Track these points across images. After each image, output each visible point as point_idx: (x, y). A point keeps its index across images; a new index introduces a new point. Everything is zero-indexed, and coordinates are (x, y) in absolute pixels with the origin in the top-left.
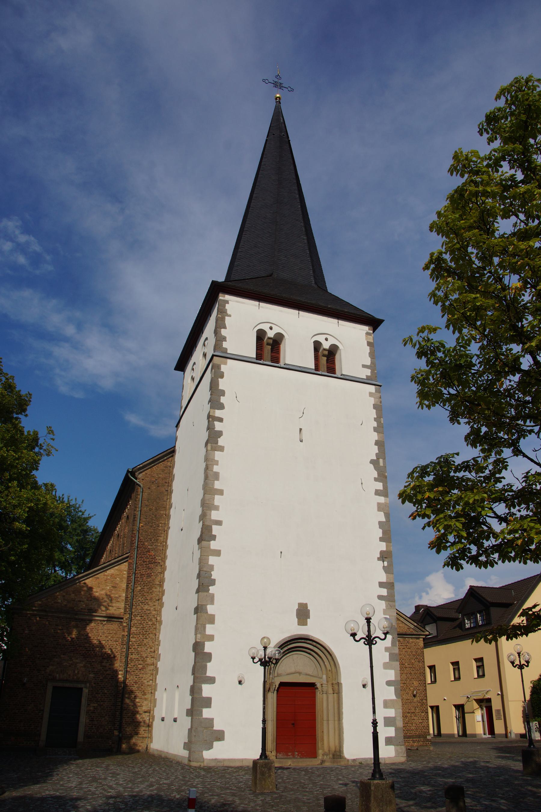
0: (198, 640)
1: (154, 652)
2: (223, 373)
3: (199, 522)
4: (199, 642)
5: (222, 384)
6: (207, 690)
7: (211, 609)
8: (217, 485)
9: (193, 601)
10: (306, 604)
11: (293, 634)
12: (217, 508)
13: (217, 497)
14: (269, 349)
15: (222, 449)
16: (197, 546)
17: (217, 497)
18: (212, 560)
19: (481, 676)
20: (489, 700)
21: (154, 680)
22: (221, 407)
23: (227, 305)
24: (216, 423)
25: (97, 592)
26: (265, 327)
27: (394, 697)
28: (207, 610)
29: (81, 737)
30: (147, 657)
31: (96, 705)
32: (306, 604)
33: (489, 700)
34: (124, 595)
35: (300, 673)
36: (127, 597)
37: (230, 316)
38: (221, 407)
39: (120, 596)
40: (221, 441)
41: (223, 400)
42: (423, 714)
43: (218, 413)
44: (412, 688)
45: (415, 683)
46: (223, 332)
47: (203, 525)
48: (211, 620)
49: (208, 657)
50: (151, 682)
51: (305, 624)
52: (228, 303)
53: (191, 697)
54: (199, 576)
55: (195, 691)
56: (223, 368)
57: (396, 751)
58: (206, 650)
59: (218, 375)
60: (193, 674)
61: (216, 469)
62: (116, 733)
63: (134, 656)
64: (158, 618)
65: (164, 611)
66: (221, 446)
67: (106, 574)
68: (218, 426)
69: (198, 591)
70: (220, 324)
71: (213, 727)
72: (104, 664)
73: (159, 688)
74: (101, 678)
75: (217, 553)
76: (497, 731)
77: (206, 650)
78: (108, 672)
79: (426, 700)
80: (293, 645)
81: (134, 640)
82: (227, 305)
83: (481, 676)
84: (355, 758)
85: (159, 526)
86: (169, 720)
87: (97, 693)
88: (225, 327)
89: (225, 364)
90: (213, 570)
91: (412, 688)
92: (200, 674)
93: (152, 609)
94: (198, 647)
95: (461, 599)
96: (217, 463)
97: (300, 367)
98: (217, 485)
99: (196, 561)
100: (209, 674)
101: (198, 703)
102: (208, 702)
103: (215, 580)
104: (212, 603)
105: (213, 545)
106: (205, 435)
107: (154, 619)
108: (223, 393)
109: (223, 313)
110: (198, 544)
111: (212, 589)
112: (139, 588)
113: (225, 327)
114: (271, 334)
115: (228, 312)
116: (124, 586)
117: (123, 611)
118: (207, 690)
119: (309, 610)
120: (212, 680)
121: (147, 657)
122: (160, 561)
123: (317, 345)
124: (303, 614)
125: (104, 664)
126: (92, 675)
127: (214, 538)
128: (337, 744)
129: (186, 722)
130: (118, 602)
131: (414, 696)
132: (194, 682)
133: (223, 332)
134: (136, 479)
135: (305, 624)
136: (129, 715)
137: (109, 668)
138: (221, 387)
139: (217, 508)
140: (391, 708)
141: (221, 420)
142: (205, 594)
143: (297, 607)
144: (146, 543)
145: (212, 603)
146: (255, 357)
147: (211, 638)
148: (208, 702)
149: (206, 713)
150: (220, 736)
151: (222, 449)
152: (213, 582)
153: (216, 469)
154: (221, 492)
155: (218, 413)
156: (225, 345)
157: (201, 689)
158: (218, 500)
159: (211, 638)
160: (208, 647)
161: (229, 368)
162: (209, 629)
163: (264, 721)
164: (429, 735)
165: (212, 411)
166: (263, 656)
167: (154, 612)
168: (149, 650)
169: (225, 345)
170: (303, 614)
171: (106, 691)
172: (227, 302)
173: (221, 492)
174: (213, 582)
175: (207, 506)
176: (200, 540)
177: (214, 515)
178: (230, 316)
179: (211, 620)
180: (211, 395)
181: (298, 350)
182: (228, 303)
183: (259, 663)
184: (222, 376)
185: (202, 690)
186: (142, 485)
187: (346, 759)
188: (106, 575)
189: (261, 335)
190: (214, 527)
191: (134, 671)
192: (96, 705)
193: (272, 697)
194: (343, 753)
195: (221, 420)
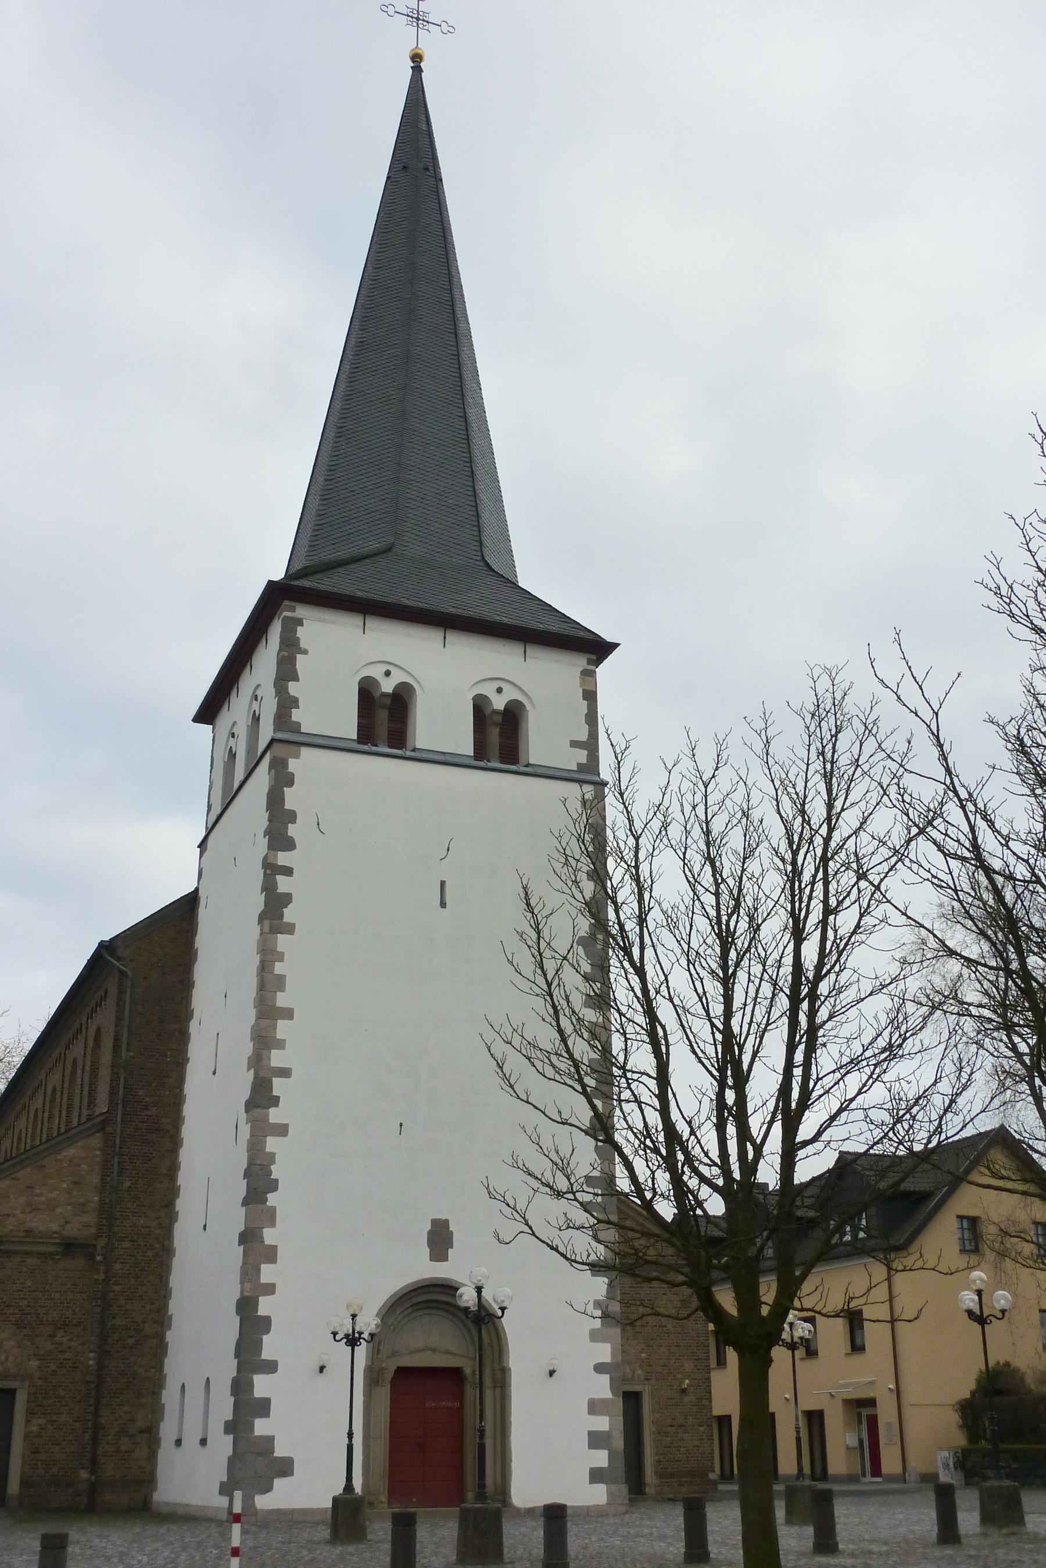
0: (246, 1294)
1: (159, 1311)
2: (293, 775)
3: (249, 1070)
4: (248, 1298)
5: (292, 798)
6: (262, 1385)
7: (270, 1236)
8: (282, 1000)
9: (237, 1219)
10: (446, 1222)
11: (421, 1278)
12: (281, 1045)
13: (280, 1023)
14: (385, 719)
15: (290, 929)
16: (243, 1116)
17: (280, 1023)
18: (272, 1144)
19: (857, 1347)
20: (871, 1402)
21: (159, 1366)
22: (289, 845)
23: (299, 628)
24: (280, 878)
25: (41, 1195)
26: (376, 672)
27: (608, 1394)
28: (262, 1237)
29: (14, 1486)
30: (143, 1322)
31: (43, 1421)
32: (446, 1222)
33: (871, 1402)
34: (96, 1198)
35: (434, 1350)
36: (102, 1203)
37: (305, 652)
38: (289, 845)
39: (88, 1201)
40: (289, 914)
41: (292, 830)
42: (702, 1429)
43: (283, 858)
44: (679, 1376)
45: (686, 1365)
46: (293, 688)
47: (255, 1078)
48: (271, 1255)
49: (265, 1324)
50: (153, 1370)
51: (445, 1258)
52: (302, 625)
53: (233, 1399)
54: (247, 1174)
55: (241, 1387)
56: (293, 765)
57: (610, 1494)
58: (262, 1311)
59: (282, 779)
60: (237, 1356)
61: (279, 968)
62: (84, 1474)
63: (118, 1322)
64: (166, 1243)
65: (178, 1229)
66: (289, 924)
67: (59, 1157)
68: (283, 884)
69: (246, 1202)
70: (286, 672)
71: (273, 1452)
72: (57, 1339)
73: (169, 1382)
74: (53, 1367)
75: (282, 1130)
76: (885, 1469)
77: (262, 1311)
78: (67, 1355)
79: (710, 1400)
80: (430, 1299)
81: (117, 1288)
82: (299, 628)
83: (857, 1347)
84: (532, 1505)
85: (166, 1056)
86: (191, 1440)
87: (44, 1398)
88: (296, 678)
89: (297, 756)
90: (274, 1163)
91: (679, 1376)
92: (249, 1357)
93: (154, 1224)
94: (246, 1306)
95: (829, 1171)
96: (281, 957)
97: (444, 753)
98: (282, 1000)
99: (243, 1145)
100: (266, 1355)
101: (248, 1407)
102: (263, 1408)
103: (277, 1181)
104: (272, 1223)
105: (275, 1115)
106: (258, 901)
107: (157, 1246)
108: (292, 817)
109: (290, 647)
110: (246, 1112)
111: (272, 1199)
112: (128, 1184)
113: (296, 678)
114: (388, 686)
115: (303, 645)
116: (96, 1180)
117: (94, 1230)
118: (262, 1385)
119: (452, 1232)
120: (271, 1367)
121: (143, 1322)
122: (169, 1127)
123: (480, 706)
124: (440, 1240)
125: (57, 1339)
126: (34, 1363)
127: (275, 1101)
128: (499, 1481)
129: (223, 1445)
130: (85, 1212)
131: (684, 1391)
132: (239, 1370)
133: (293, 688)
134: (118, 959)
135: (445, 1258)
136: (109, 1437)
137: (69, 1348)
138: (288, 806)
139: (281, 1045)
140: (603, 1414)
141: (288, 871)
142: (260, 1207)
143: (428, 1227)
144: (141, 1093)
145: (272, 1223)
146: (355, 737)
147: (270, 1289)
148: (263, 1408)
149: (261, 1427)
150: (285, 1467)
151: (290, 929)
152: (274, 1185)
153: (279, 968)
154: (288, 1014)
155: (283, 858)
156: (296, 715)
157: (251, 1385)
158: (283, 1029)
159: (270, 1289)
160: (265, 1306)
161: (304, 764)
162: (267, 1273)
163: (350, 1435)
164: (713, 1471)
165: (272, 853)
166: (351, 1331)
167: (157, 1231)
168: (148, 1307)
169: (296, 715)
170: (440, 1240)
171: (62, 1393)
172: (300, 622)
173: (288, 1014)
174: (274, 1185)
175: (264, 1041)
176: (251, 1105)
177: (277, 1059)
178: (305, 652)
179: (271, 1255)
180: (270, 820)
181: (442, 726)
182: (302, 625)
183: (345, 1340)
184: (290, 783)
185: (253, 1385)
186: (129, 973)
187: (515, 1507)
188: (60, 1160)
189: (367, 692)
190: (276, 1081)
191: (118, 1352)
192: (43, 1421)
193: (384, 1394)
194: (510, 1497)
195: (288, 871)
